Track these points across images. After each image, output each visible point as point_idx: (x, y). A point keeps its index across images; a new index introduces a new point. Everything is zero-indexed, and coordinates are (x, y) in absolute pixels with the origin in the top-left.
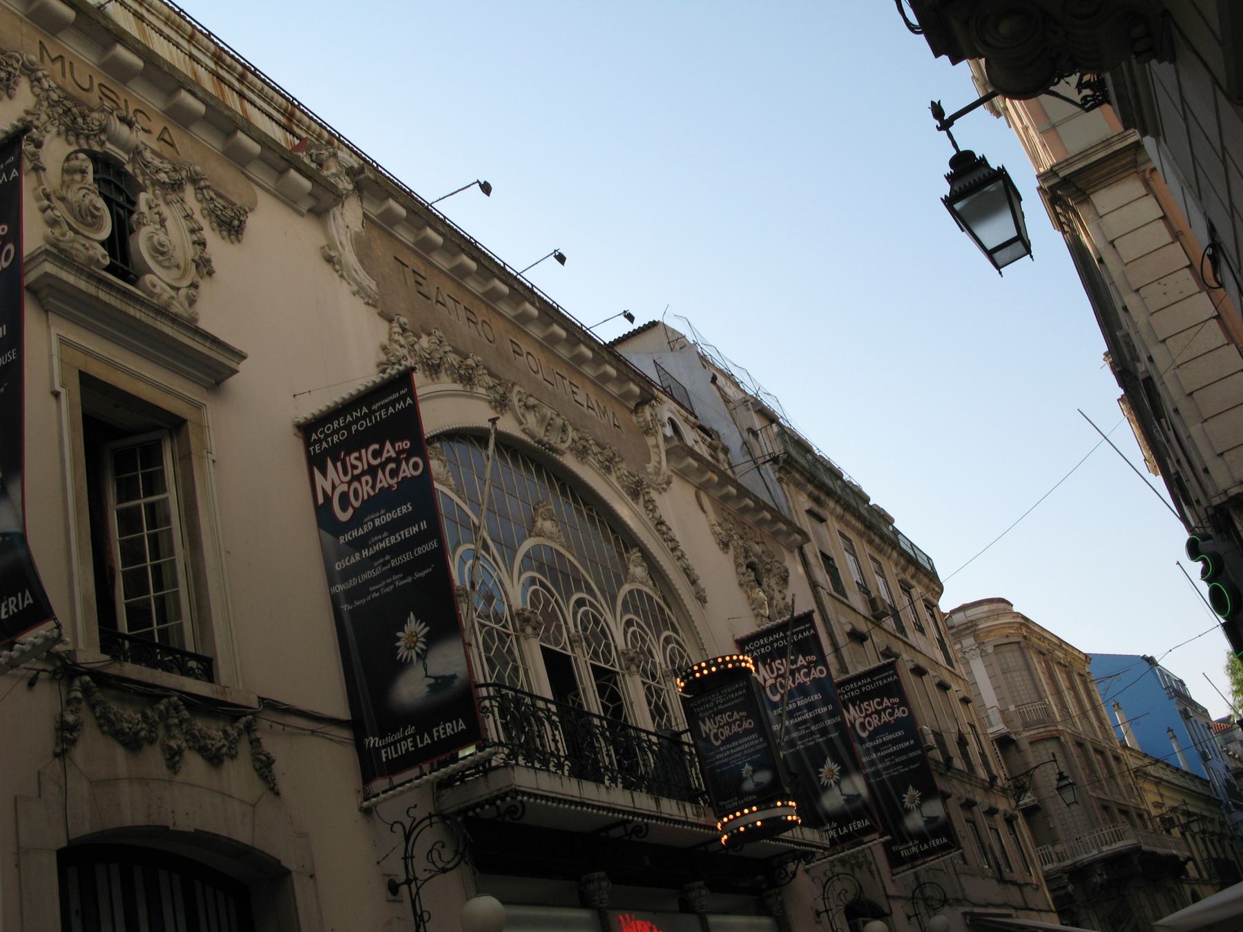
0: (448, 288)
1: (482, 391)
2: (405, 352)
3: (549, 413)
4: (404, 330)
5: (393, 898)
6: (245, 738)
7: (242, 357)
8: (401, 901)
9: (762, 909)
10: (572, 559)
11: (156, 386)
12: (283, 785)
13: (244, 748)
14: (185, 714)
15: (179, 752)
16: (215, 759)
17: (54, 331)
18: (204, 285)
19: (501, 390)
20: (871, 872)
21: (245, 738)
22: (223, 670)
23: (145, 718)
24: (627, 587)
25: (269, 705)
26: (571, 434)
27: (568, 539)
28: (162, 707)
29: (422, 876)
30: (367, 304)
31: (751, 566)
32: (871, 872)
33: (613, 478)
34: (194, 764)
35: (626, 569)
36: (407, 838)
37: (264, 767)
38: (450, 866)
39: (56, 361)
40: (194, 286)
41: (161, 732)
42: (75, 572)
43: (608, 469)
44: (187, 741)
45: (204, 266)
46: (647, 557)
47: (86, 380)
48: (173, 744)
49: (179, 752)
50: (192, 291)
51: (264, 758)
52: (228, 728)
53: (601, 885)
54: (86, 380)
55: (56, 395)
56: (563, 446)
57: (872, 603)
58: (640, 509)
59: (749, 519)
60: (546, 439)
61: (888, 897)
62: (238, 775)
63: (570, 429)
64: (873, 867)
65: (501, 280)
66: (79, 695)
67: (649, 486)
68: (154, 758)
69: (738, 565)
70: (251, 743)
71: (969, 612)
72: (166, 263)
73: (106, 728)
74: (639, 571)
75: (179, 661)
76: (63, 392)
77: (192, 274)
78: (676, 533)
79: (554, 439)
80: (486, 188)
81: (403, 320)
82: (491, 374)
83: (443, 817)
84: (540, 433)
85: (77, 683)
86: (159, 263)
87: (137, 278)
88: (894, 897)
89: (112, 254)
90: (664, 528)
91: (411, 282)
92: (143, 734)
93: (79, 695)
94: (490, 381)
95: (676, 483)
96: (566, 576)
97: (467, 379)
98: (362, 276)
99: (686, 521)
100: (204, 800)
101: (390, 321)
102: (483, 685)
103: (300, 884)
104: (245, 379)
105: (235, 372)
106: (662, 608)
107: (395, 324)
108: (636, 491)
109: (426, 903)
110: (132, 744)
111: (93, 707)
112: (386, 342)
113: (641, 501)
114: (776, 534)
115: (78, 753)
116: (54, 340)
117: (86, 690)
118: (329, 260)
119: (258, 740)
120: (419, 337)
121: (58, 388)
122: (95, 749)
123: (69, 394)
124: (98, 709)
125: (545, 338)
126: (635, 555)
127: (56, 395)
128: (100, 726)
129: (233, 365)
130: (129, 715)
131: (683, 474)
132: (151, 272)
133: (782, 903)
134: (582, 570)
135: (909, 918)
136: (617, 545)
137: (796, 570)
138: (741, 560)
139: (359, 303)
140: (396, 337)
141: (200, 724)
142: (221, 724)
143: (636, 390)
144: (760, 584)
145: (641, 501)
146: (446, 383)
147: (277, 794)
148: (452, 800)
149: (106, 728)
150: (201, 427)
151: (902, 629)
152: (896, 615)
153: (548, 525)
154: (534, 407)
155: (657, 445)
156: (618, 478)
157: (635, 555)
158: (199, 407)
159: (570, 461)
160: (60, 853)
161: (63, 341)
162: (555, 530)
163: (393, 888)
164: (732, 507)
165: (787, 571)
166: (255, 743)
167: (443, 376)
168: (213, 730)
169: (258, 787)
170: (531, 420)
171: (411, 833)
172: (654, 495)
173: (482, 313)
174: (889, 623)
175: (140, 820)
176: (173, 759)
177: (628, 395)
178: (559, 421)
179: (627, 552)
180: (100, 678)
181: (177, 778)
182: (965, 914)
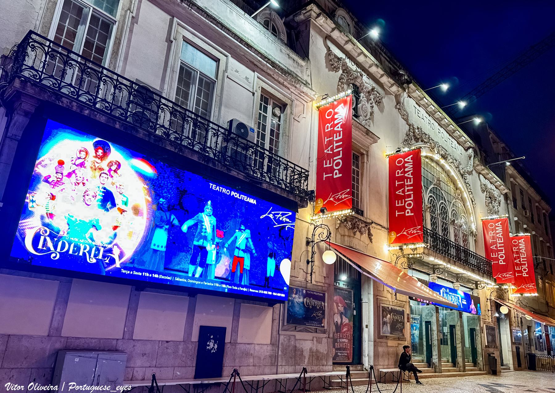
16: (362, 234)
37: (370, 235)
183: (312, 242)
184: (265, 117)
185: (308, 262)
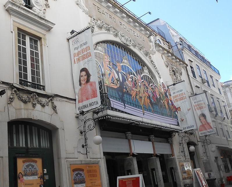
0: (105, 10)
1: (112, 33)
2: (94, 24)
3: (127, 37)
4: (94, 19)
5: (81, 134)
6: (50, 102)
7: (55, 24)
8: (83, 135)
9: (168, 142)
10: (131, 68)
11: (24, 26)
12: (58, 111)
13: (50, 104)
14: (37, 97)
15: (35, 104)
16: (43, 106)
17: (12, 19)
18: (47, 10)
19: (116, 32)
20: (194, 136)
21: (50, 102)
22: (46, 88)
23: (28, 97)
24: (143, 74)
25: (57, 96)
26: (132, 42)
27: (130, 64)
28: (32, 95)
29: (87, 131)
30: (86, 14)
31: (173, 71)
32: (194, 136)
33: (142, 51)
34: (38, 107)
35: (143, 71)
36: (85, 123)
37: (54, 108)
38: (93, 129)
39: (12, 25)
40: (45, 10)
41: (32, 100)
42: (14, 67)
43: (141, 50)
44: (37, 102)
45: (47, 6)
46: (148, 68)
47: (19, 29)
48: (34, 103)
49: (35, 104)
50: (44, 11)
51: (54, 106)
52: (47, 100)
53: (129, 134)
54: (19, 29)
55: (12, 32)
56: (130, 45)
57: (202, 80)
58: (148, 58)
59: (174, 61)
60: (126, 43)
61: (198, 141)
62: (48, 109)
63: (132, 41)
64: (195, 135)
65: (110, 3)
66: (14, 92)
67: (150, 53)
68: (30, 105)
69: (170, 71)
70: (52, 103)
71: (228, 83)
72: (38, 5)
73: (19, 99)
74: (146, 71)
75: (38, 86)
76: (13, 31)
77: (45, 7)
78: (156, 63)
79: (128, 43)
80: (150, 13)
81: (94, 17)
82: (114, 29)
83: (94, 120)
84: (125, 42)
85: (13, 90)
86: (37, 5)
87: (32, 8)
88: (199, 141)
89: (26, 3)
90: (153, 62)
91: (97, 9)
92: (27, 100)
93: (14, 92)
94: (114, 30)
95: (157, 52)
96: (149, 81)
97: (108, 30)
98: (86, 9)
99: (158, 61)
100: (40, 113)
101: (91, 17)
102: (104, 93)
103: (60, 131)
104: (55, 29)
105: (52, 28)
106: (150, 80)
107: (92, 18)
108: (147, 54)
109: (87, 136)
110: (25, 102)
111: (17, 95)
112: (90, 22)
113: (148, 57)
114: (180, 64)
115: (13, 103)
116: (12, 20)
117: (15, 91)
118: (77, 4)
119: (53, 102)
120: (98, 21)
121: (12, 31)
122: (17, 103)
123: (15, 32)
124: (18, 95)
125: (140, 30)
126: (146, 68)
127: (12, 32)
128: (18, 98)
129: (52, 26)
130: (25, 96)
131: (159, 51)
132: (35, 7)
133: (172, 141)
134: (133, 70)
135: (202, 146)
136: (142, 66)
137: (183, 71)
138: (171, 70)
139: (84, 13)
140: (92, 21)
141: (40, 99)
142: (27, 95)
143: (149, 33)
144: (175, 75)
145: (148, 57)
146: (103, 31)
147: (57, 113)
148: (96, 116)
149: (19, 99)
150: (45, 39)
151: (209, 85)
152: (208, 82)
153: (125, 61)
154: (124, 36)
155: (152, 44)
156: (143, 52)
157: (146, 68)
158: (45, 35)
159: (132, 48)
160: (8, 122)
161: (14, 21)
162: (127, 62)
163: (81, 133)
164: (170, 58)
165: (182, 72)
166: (53, 103)
167: (103, 29)
168: (44, 100)
169: (53, 111)
170: (123, 39)
171: (85, 122)
172: (151, 55)
173: (113, 16)
174: (206, 84)
175: (26, 117)
176: (34, 105)
177: (147, 34)
178: (129, 39)
179: (144, 67)
180: (18, 89)
181: (35, 109)
182: (217, 146)
183: (84, 132)
184: (24, 50)
185: (83, 146)
